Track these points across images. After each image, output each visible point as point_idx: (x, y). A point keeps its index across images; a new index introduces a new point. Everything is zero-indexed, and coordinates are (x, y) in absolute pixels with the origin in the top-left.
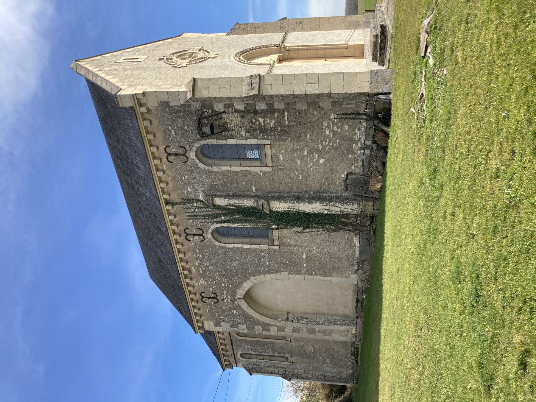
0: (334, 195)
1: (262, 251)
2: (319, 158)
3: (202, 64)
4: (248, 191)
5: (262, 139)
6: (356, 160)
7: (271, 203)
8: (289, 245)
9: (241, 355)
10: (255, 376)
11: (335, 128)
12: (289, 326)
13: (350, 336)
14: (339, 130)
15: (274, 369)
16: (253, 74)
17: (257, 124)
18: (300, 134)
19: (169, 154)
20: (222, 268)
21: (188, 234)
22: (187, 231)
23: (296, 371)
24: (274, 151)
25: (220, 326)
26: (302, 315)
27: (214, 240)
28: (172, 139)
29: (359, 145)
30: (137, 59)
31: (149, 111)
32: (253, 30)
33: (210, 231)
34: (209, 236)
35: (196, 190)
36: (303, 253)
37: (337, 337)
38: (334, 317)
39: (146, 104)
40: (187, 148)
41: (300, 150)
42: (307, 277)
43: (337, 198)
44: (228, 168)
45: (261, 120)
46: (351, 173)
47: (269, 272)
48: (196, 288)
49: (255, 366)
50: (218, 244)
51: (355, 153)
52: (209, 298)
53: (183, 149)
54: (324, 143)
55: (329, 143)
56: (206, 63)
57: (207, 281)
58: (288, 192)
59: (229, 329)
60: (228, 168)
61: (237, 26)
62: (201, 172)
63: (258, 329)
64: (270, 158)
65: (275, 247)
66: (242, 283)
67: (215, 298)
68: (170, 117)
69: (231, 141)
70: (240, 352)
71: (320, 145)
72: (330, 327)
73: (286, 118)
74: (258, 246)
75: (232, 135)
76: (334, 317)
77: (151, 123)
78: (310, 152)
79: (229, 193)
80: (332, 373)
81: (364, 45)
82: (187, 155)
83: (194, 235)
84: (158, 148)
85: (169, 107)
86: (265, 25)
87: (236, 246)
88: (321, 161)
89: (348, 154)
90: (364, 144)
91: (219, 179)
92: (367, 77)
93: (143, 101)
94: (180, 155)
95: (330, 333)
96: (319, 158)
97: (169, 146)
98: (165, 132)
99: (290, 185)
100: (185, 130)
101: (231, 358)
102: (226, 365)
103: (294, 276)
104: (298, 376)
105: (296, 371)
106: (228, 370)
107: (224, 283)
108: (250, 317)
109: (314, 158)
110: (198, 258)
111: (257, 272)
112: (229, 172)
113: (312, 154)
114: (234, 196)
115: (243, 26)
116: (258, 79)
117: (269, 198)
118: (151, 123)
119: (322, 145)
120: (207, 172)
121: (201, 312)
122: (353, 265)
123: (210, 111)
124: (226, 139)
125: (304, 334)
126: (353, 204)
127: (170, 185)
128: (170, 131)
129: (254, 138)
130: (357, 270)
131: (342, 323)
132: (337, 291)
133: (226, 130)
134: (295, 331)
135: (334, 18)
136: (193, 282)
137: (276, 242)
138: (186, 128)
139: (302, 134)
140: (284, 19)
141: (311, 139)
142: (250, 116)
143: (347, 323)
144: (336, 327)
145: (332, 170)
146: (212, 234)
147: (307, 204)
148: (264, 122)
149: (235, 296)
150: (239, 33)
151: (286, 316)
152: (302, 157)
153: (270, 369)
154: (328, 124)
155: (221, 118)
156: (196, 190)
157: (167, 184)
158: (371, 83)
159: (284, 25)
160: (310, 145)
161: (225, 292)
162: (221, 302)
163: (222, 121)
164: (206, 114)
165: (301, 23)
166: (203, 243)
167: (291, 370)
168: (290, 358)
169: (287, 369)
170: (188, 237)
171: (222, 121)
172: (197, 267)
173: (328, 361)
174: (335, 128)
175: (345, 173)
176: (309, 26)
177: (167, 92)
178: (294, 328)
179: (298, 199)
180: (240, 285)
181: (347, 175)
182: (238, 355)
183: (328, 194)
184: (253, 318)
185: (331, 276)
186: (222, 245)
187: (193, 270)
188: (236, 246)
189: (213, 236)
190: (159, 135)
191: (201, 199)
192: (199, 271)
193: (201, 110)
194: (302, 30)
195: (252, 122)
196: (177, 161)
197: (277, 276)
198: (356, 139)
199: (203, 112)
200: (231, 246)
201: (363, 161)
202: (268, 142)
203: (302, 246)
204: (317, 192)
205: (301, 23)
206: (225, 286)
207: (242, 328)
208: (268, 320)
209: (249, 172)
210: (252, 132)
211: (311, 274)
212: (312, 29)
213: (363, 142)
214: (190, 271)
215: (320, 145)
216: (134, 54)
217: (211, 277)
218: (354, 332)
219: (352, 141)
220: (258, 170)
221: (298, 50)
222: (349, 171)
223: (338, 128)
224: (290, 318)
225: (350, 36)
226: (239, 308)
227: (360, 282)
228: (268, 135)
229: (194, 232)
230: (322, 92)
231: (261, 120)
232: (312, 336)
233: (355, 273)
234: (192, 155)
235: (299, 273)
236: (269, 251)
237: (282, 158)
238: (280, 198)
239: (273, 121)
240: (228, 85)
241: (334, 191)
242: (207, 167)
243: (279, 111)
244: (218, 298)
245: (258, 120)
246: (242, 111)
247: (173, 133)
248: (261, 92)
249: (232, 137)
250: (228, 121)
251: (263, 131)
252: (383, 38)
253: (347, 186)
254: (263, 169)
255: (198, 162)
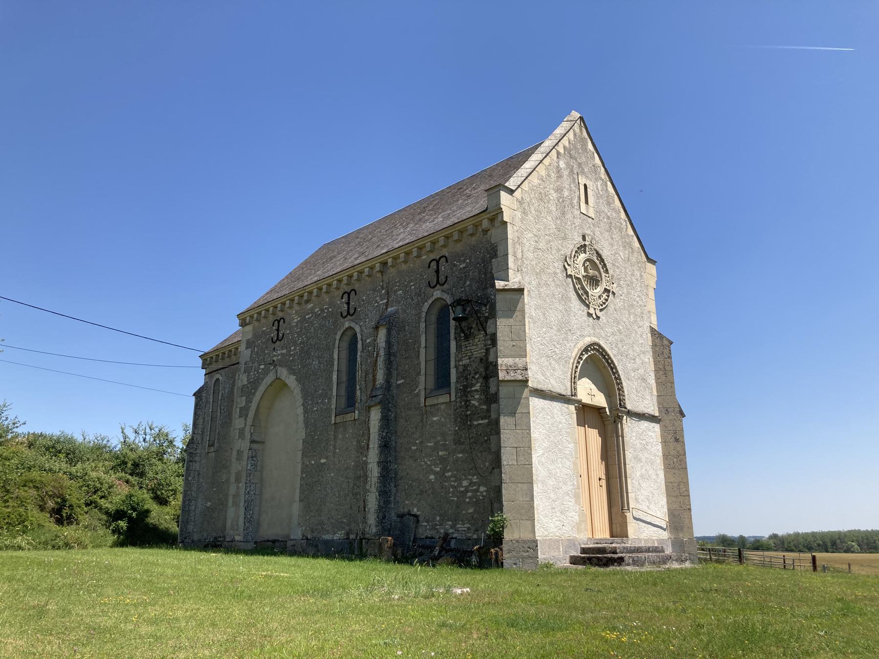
0: (392, 499)
1: (330, 399)
2: (436, 473)
3: (574, 297)
4: (398, 375)
5: (456, 388)
6: (433, 528)
7: (379, 407)
8: (335, 438)
9: (218, 380)
10: (193, 400)
11: (469, 494)
12: (244, 445)
13: (232, 532)
14: (467, 500)
15: (200, 427)
16: (529, 372)
17: (474, 382)
18: (463, 443)
19: (438, 262)
20: (311, 345)
21: (349, 294)
22: (353, 292)
23: (197, 459)
24: (443, 407)
25: (247, 348)
26: (259, 463)
27: (342, 331)
28: (455, 266)
29: (451, 531)
30: (587, 202)
31: (485, 231)
32: (661, 367)
33: (353, 325)
34: (347, 325)
35: (399, 302)
36: (327, 458)
37: (231, 513)
38: (257, 509)
39: (493, 226)
40: (446, 286)
41: (444, 445)
42: (300, 466)
43: (387, 502)
44: (423, 344)
45: (477, 387)
46: (418, 521)
47: (306, 412)
48: (290, 311)
49: (204, 400)
50: (338, 337)
51: (441, 525)
52: (278, 330)
53: (444, 280)
54: (452, 479)
55: (453, 486)
56: (575, 303)
57: (297, 326)
58: (396, 432)
59: (242, 361)
60: (423, 344)
61: (666, 342)
62: (419, 306)
63: (241, 402)
64: (436, 402)
65: (333, 418)
66: (294, 374)
67: (278, 339)
68: (479, 260)
69: (453, 344)
70: (221, 378)
71: (450, 474)
72: (242, 504)
73: (481, 422)
74: (334, 394)
75: (461, 346)
76: (257, 509)
77: (472, 235)
78: (443, 460)
79: (395, 348)
80: (194, 511)
81: (627, 537)
82: (438, 286)
83: (348, 304)
84: (444, 246)
85: (491, 258)
86: (669, 385)
87: (336, 363)
88: (432, 477)
89: (440, 515)
90: (452, 538)
91: (411, 333)
92: (527, 536)
93: (497, 223)
94: (438, 278)
95: (236, 504)
96: (436, 473)
97: (447, 261)
98: (463, 255)
99: (405, 434)
100: (465, 283)
101: (214, 367)
102: (208, 360)
103: (300, 447)
104: (191, 461)
105: (197, 459)
106: (200, 361)
107: (295, 349)
108: (256, 389)
109: (436, 465)
110: (322, 310)
111: (306, 394)
112: (419, 346)
113: (440, 463)
114: (389, 354)
115: (666, 351)
116: (520, 378)
117: (387, 406)
118: (472, 235)
119: (450, 477)
120: (419, 315)
121: (263, 321)
122: (313, 532)
123: (487, 315)
124: (456, 338)
125: (235, 467)
126: (377, 526)
127: (404, 267)
128: (464, 261)
129: (458, 378)
130: (307, 539)
131: (248, 520)
132: (285, 513)
133: (467, 338)
134: (240, 453)
135: (687, 490)
136: (296, 307)
137: (339, 419)
138: (468, 283)
139: (463, 447)
140: (683, 415)
141: (457, 460)
142: (482, 370)
143: (248, 527)
144: (242, 512)
145: (422, 492)
146: (350, 328)
147: (377, 460)
148: (476, 390)
149: (280, 366)
150: (654, 346)
151: (258, 439)
152: (435, 449)
153: (201, 421)
154: (475, 484)
155: (479, 330)
156: (399, 302)
157: (405, 262)
158: (517, 541)
159: (670, 417)
160: (451, 459)
161: (284, 351)
162: (273, 346)
163: (476, 332)
164: (484, 309)
165: (677, 440)
166: (339, 316)
167: (198, 451)
168: (212, 449)
169: (200, 446)
170: (346, 296)
171: (476, 332)
172: (312, 311)
173: (209, 504)
174: (469, 494)
175: (418, 513)
176: (672, 452)
177: (507, 255)
178: (242, 452)
179: (385, 446)
180: (292, 372)
181: (415, 516)
182: (217, 376)
183: (394, 490)
184: (255, 393)
185: (301, 501)
186: (337, 342)
187: (310, 306)
188: (336, 363)
189: (347, 329)
190: (459, 248)
191: (389, 310)
192: (308, 314)
193: (488, 302)
194: (664, 442)
195: (476, 374)
196: (430, 275)
197: (301, 424)
198: (458, 526)
199: (485, 305)
200: (336, 356)
201: (432, 538)
202: (453, 398)
203: (334, 457)
204: (396, 474)
205: (677, 440)
206: (290, 351)
207: (243, 379)
208: (251, 414)
209: (419, 374)
210: (464, 374)
211: (302, 472)
212: (666, 456)
213: (454, 536)
214: (307, 302)
215: (450, 474)
216: (598, 197)
217: (301, 331)
218: (237, 538)
219: (455, 521)
220: (421, 386)
221: (618, 437)
222: (421, 519)
223: (470, 498)
224: (255, 446)
225: (649, 519)
226: (266, 372)
227: (292, 543)
228: (461, 398)
229: (352, 303)
230: (503, 471)
231: (477, 387)
232: (233, 479)
233: (303, 536)
234: (437, 294)
235: (304, 454)
236: (329, 410)
237: (435, 419)
238: (386, 421)
239: (477, 404)
240: (514, 337)
241: (397, 499)
242: (424, 314)
243: (489, 410)
244: (278, 342)
245: (477, 382)
246: (487, 359)
247: (462, 266)
248: (503, 384)
249: (459, 347)
250: (476, 340)
251: (465, 392)
252: (604, 561)
253: (401, 516)
254: (423, 394)
255: (430, 302)
